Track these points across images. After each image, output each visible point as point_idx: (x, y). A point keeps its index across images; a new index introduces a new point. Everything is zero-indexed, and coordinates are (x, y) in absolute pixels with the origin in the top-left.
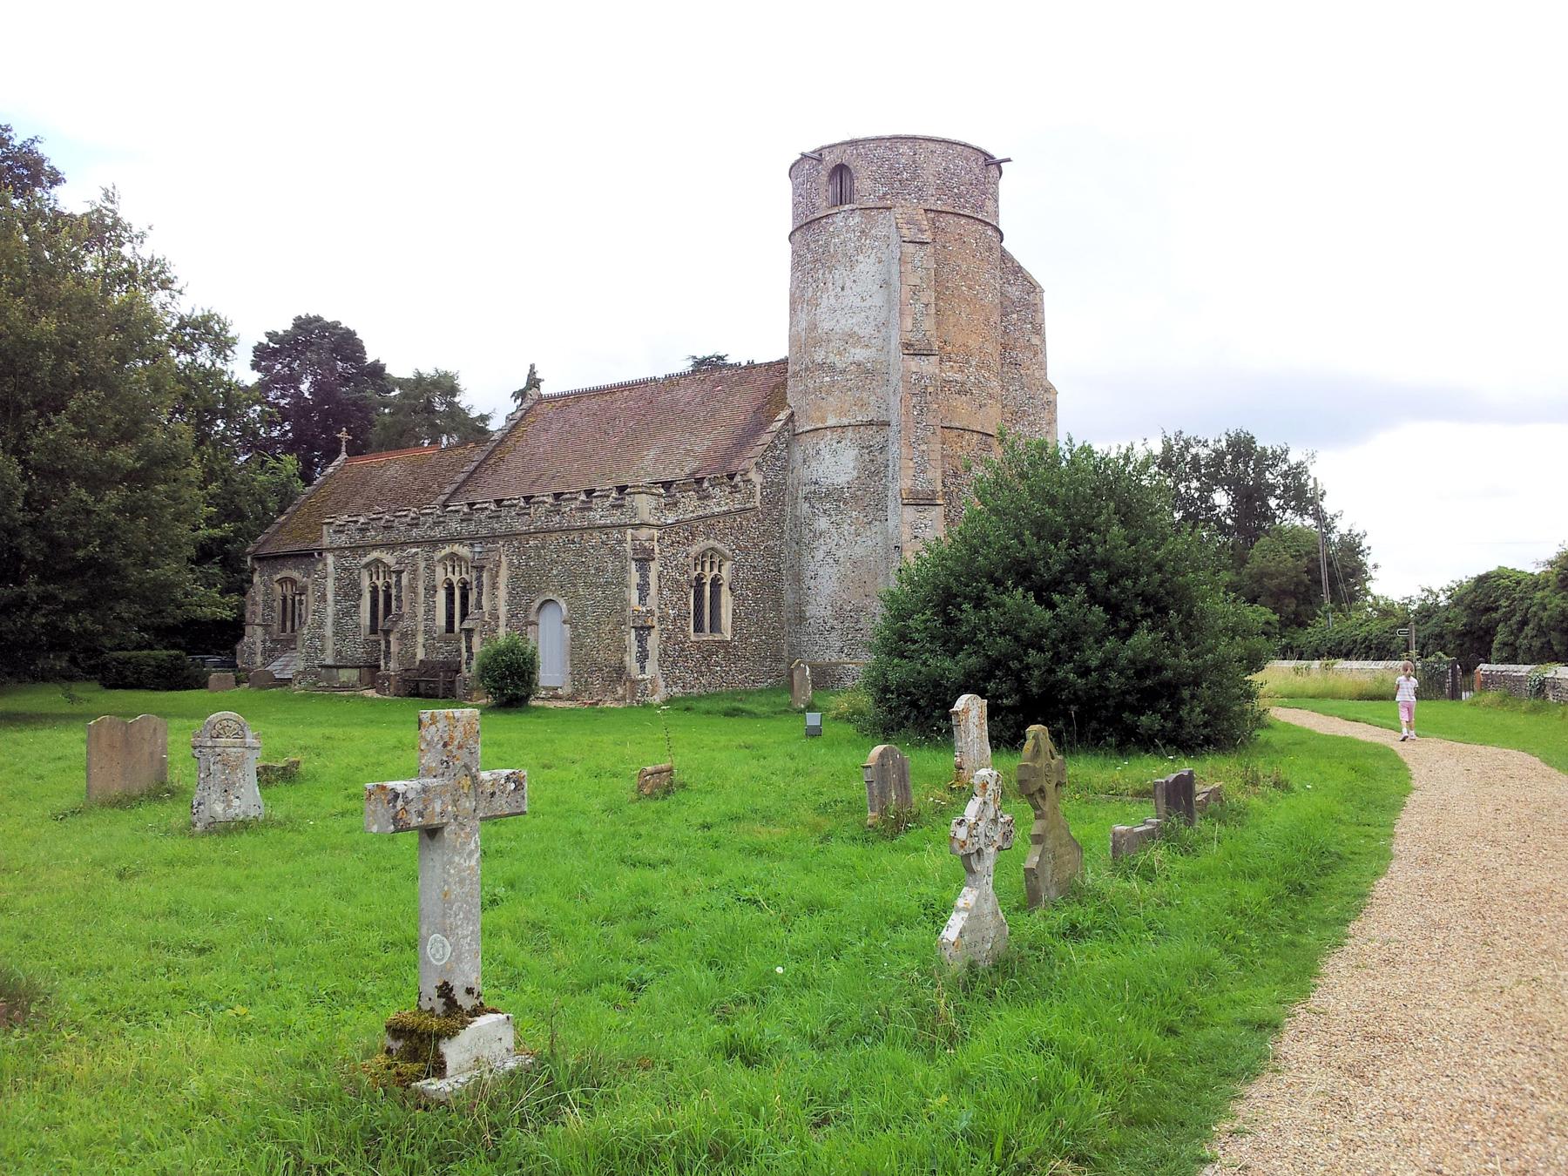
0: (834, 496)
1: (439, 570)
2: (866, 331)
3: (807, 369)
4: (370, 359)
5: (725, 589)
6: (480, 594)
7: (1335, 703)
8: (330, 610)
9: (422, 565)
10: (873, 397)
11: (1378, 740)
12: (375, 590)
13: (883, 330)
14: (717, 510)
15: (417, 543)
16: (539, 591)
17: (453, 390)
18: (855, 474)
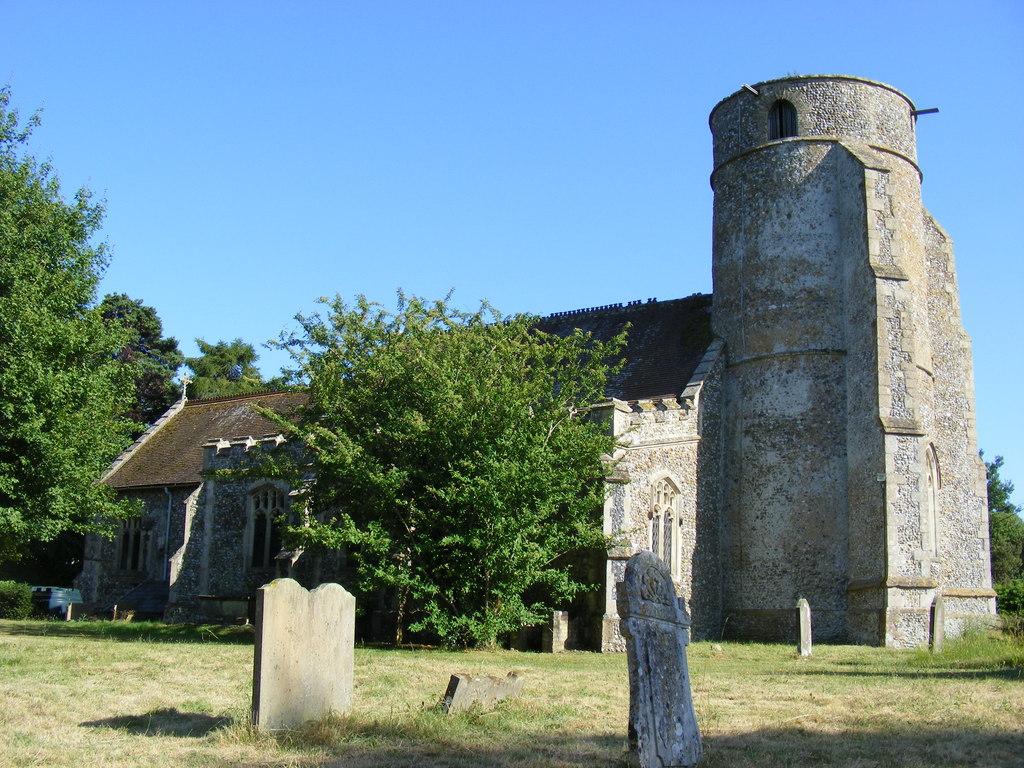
0: (787, 428)
2: (818, 259)
10: (827, 326)
14: (671, 436)
18: (810, 405)
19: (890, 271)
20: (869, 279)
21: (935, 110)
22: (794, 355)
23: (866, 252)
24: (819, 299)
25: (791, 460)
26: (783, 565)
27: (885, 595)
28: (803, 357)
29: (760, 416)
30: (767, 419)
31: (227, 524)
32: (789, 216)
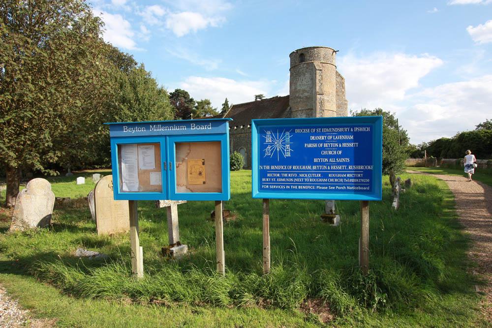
2: (308, 89)
4: (191, 98)
7: (412, 168)
17: (209, 103)
19: (320, 92)
22: (303, 110)
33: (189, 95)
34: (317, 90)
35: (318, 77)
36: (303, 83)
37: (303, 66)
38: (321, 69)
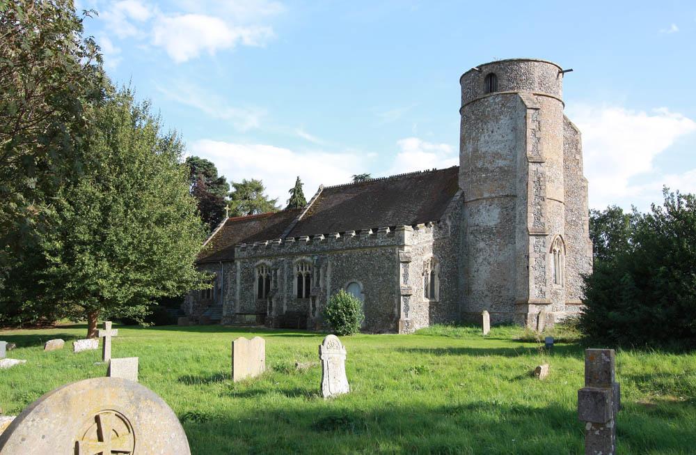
0: (488, 231)
1: (295, 269)
2: (505, 152)
3: (472, 171)
4: (219, 176)
5: (436, 277)
6: (318, 279)
8: (238, 288)
9: (286, 266)
11: (31, 331)
12: (261, 278)
13: (513, 151)
15: (283, 255)
16: (348, 278)
17: (259, 189)
18: (499, 221)
19: (536, 158)
20: (526, 162)
21: (571, 70)
22: (493, 198)
23: (525, 150)
24: (505, 171)
25: (490, 246)
26: (486, 293)
27: (528, 307)
28: (496, 199)
29: (477, 225)
30: (480, 227)
31: (246, 280)
32: (492, 132)
33: (215, 170)
34: (529, 153)
35: (531, 125)
36: (494, 139)
37: (494, 100)
38: (537, 106)
